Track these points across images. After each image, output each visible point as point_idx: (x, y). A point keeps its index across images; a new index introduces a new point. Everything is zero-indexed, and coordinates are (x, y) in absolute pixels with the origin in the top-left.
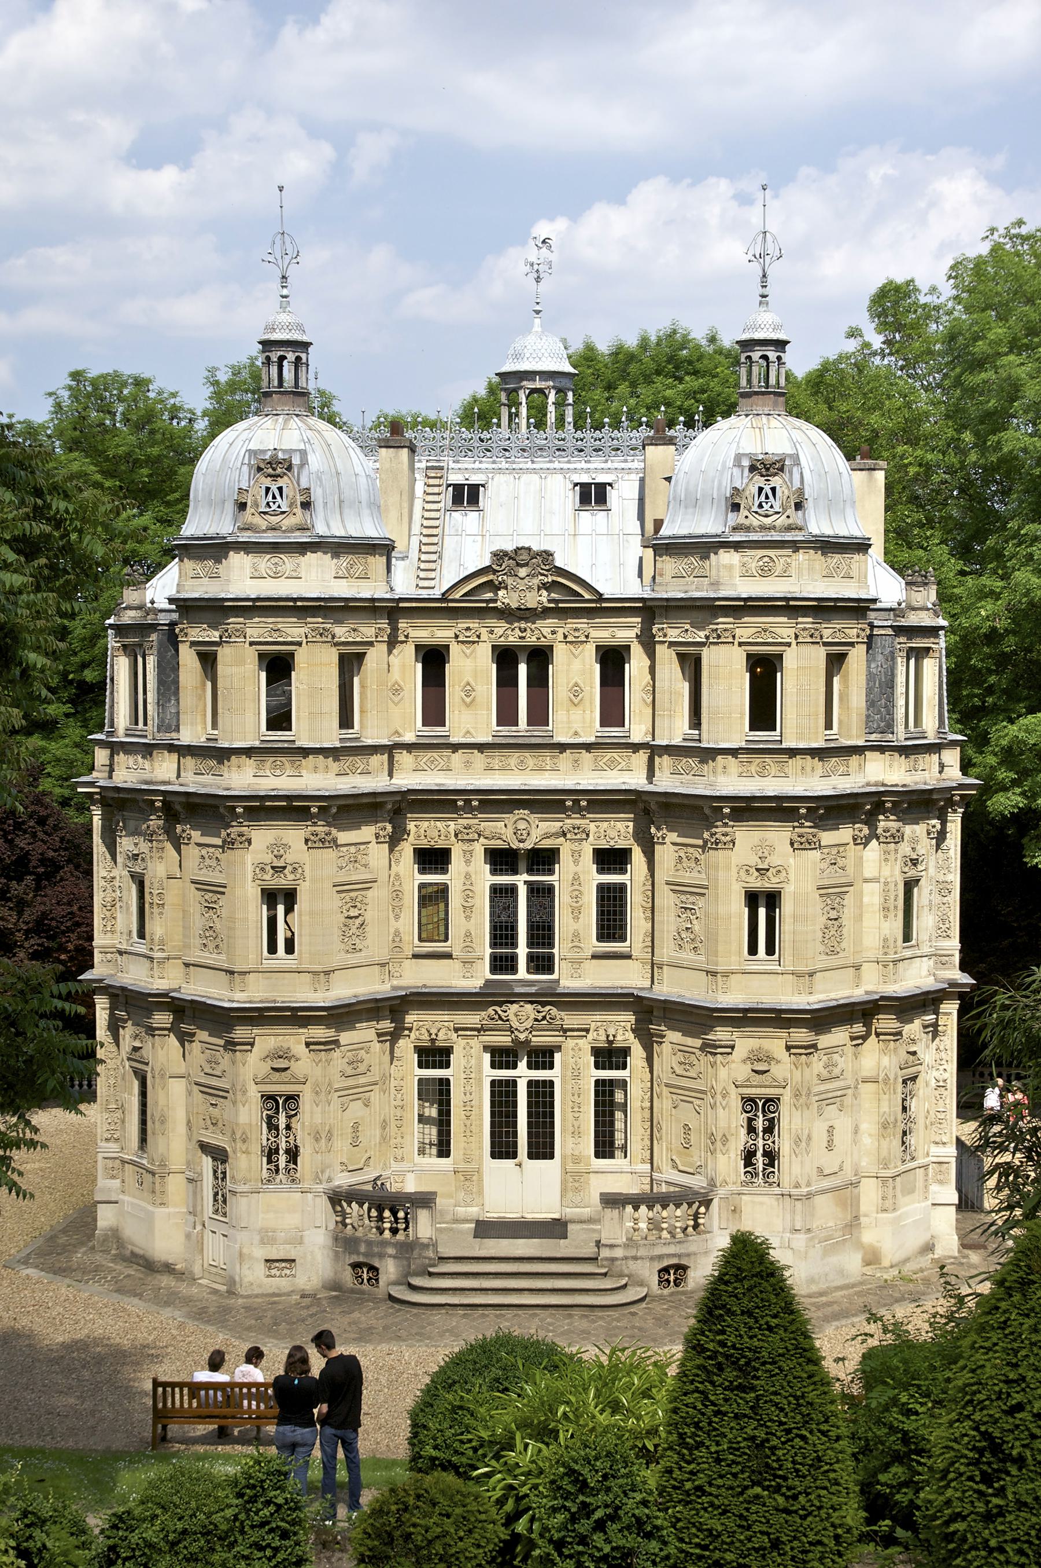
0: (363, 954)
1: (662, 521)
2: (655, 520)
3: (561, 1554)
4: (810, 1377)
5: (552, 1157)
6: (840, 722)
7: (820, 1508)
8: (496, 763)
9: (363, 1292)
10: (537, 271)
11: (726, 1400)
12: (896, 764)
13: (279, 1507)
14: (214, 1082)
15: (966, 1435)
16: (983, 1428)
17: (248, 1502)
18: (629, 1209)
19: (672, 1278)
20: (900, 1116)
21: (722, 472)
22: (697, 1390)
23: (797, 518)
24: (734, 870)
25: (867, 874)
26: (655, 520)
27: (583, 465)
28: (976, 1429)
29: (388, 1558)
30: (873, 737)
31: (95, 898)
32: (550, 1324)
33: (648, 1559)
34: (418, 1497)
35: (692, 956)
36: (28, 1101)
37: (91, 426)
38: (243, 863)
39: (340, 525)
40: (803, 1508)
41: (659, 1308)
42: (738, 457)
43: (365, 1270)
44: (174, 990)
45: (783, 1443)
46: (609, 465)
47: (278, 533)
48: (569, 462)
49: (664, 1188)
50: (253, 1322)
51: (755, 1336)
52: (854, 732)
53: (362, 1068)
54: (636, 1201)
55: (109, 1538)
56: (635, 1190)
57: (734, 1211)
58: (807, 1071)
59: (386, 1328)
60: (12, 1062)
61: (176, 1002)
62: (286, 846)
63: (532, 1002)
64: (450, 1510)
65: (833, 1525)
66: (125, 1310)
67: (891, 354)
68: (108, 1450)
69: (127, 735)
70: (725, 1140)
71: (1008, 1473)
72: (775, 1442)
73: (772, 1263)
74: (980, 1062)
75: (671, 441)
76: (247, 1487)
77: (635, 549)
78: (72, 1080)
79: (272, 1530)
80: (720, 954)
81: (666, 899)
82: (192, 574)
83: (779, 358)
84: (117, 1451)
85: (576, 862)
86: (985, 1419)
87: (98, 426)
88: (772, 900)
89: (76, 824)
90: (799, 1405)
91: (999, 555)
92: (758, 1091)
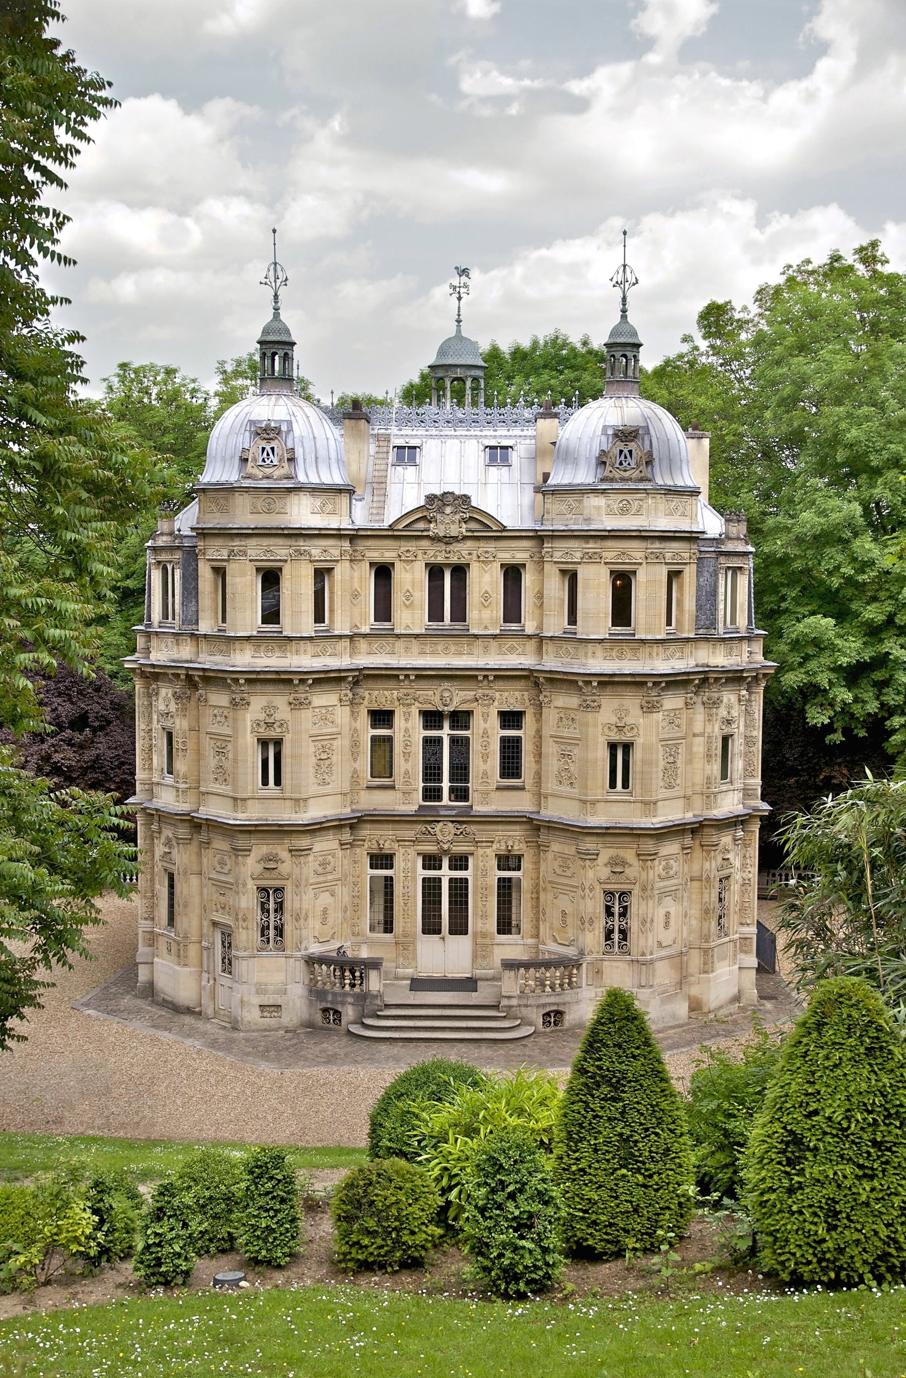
0: (330, 786)
1: (549, 474)
2: (544, 473)
3: (483, 1216)
4: (663, 1091)
5: (466, 933)
6: (677, 621)
7: (668, 1184)
8: (428, 649)
9: (330, 1029)
10: (459, 292)
11: (602, 1108)
12: (717, 651)
13: (279, 1181)
14: (223, 878)
15: (776, 1132)
16: (789, 1128)
17: (257, 1178)
18: (522, 970)
19: (552, 1020)
20: (717, 905)
21: (592, 439)
22: (581, 1101)
23: (647, 473)
24: (600, 727)
25: (697, 731)
26: (544, 473)
27: (492, 433)
28: (784, 1128)
29: (358, 1218)
30: (701, 632)
31: (137, 745)
32: (465, 1053)
33: (546, 1220)
34: (379, 1175)
35: (569, 789)
36: (93, 890)
37: (133, 403)
38: (244, 720)
39: (316, 475)
40: (657, 1184)
41: (542, 1041)
42: (605, 428)
43: (331, 1012)
44: (194, 811)
45: (643, 1138)
46: (511, 433)
47: (271, 481)
48: (481, 431)
49: (547, 956)
50: (251, 1049)
51: (623, 1062)
52: (687, 628)
53: (329, 868)
54: (527, 965)
55: (158, 1201)
56: (525, 957)
57: (597, 972)
58: (651, 872)
59: (346, 1055)
60: (82, 863)
61: (195, 820)
62: (276, 708)
63: (452, 822)
64: (402, 1184)
65: (677, 1196)
66: (158, 1040)
67: (713, 355)
68: (148, 1139)
69: (160, 627)
70: (591, 922)
71: (807, 1159)
72: (637, 1137)
73: (635, 1010)
74: (784, 866)
75: (556, 416)
76: (257, 1167)
77: (528, 495)
78: (125, 876)
79: (273, 1198)
80: (589, 788)
81: (551, 748)
82: (209, 510)
83: (635, 356)
84: (155, 1140)
85: (485, 721)
86: (790, 1121)
87: (139, 403)
88: (627, 747)
89: (122, 691)
90: (654, 1111)
91: (791, 501)
92: (616, 886)
